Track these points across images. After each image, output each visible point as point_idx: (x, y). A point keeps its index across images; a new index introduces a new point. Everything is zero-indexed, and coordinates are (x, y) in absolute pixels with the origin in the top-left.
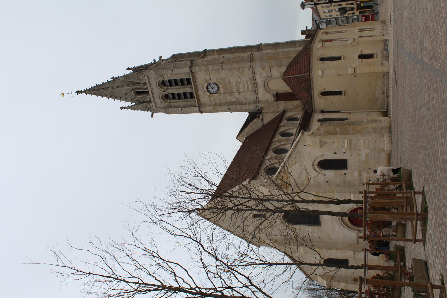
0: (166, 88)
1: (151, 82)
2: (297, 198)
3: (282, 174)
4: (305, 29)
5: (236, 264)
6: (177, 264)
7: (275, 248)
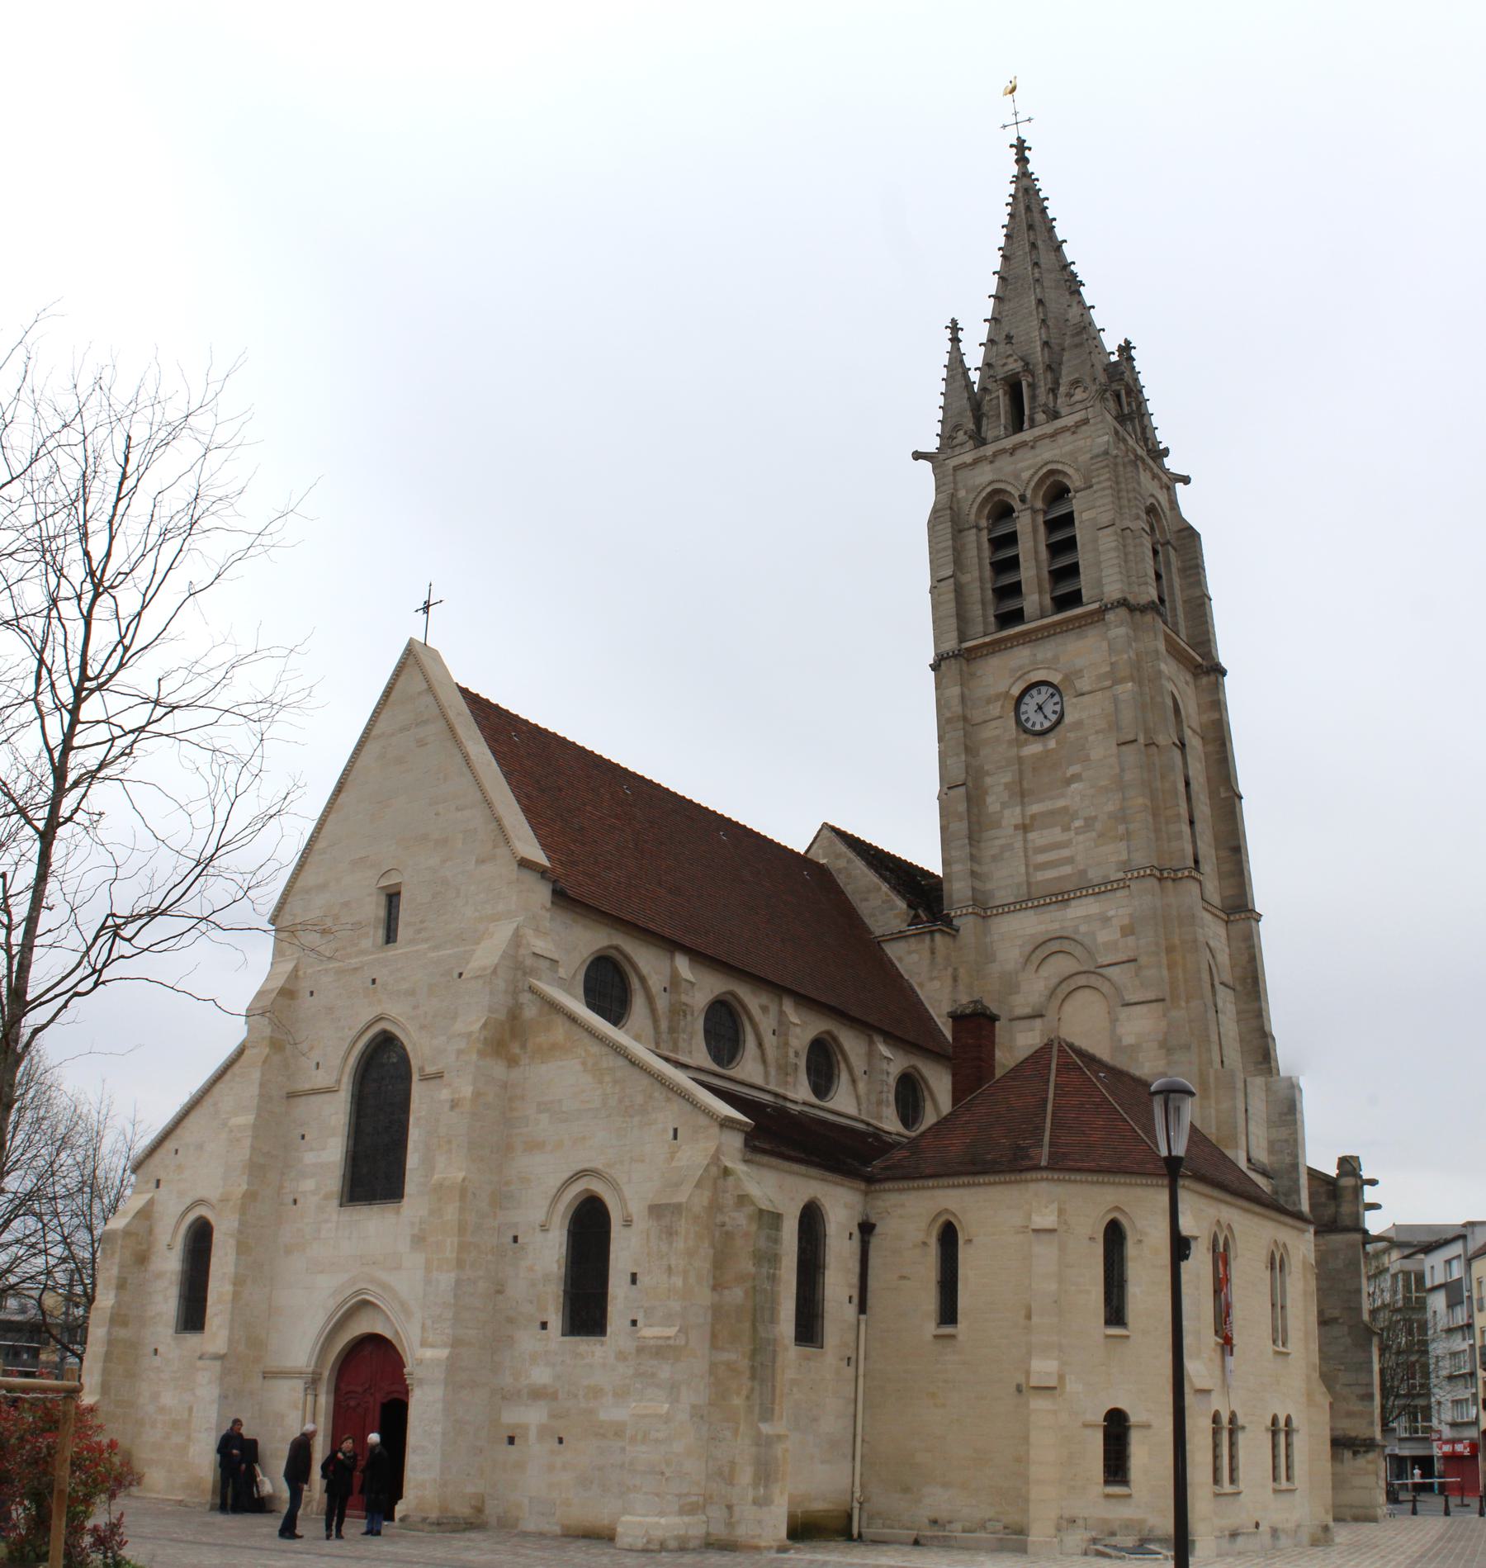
0: (1039, 505)
1: (1061, 439)
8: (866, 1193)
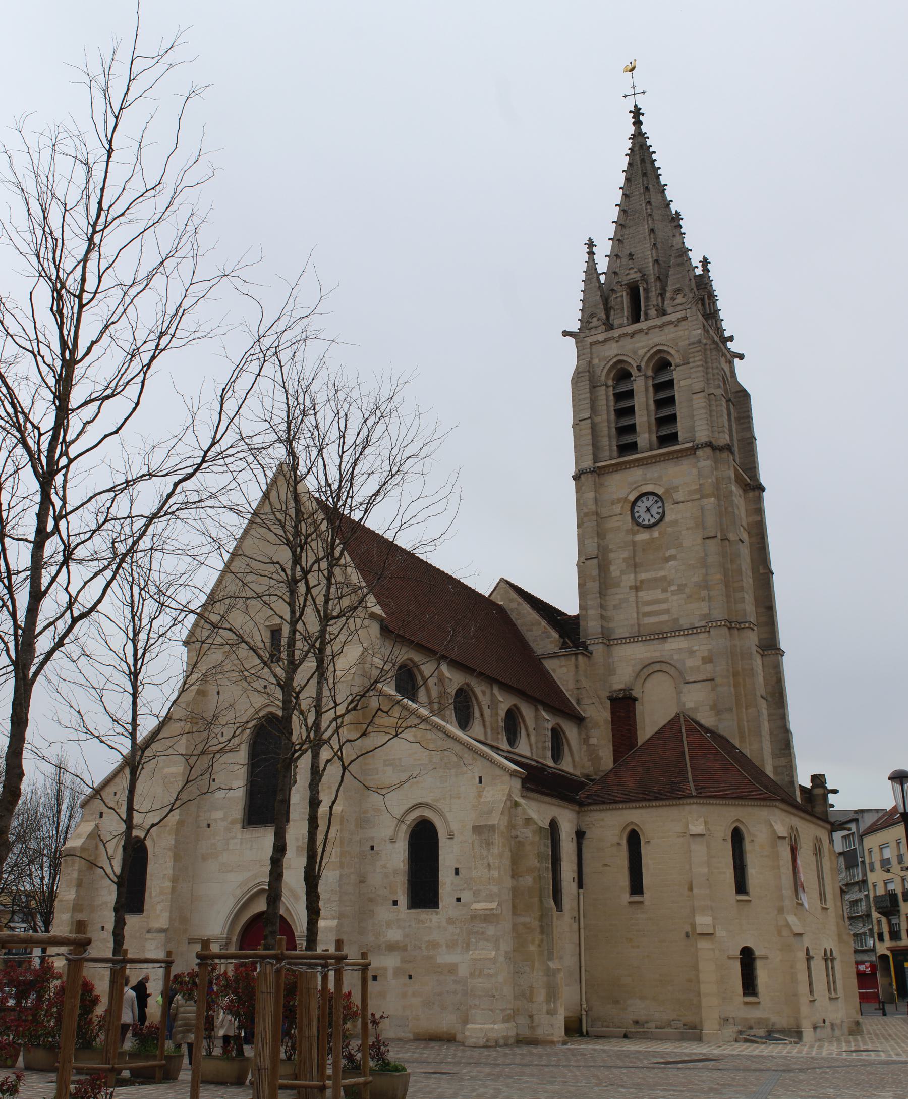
0: (650, 373)
1: (666, 329)
2: (325, 754)
3: (396, 712)
4: (830, 786)
5: (136, 576)
6: (137, 404)
7: (183, 690)
8: (578, 813)
